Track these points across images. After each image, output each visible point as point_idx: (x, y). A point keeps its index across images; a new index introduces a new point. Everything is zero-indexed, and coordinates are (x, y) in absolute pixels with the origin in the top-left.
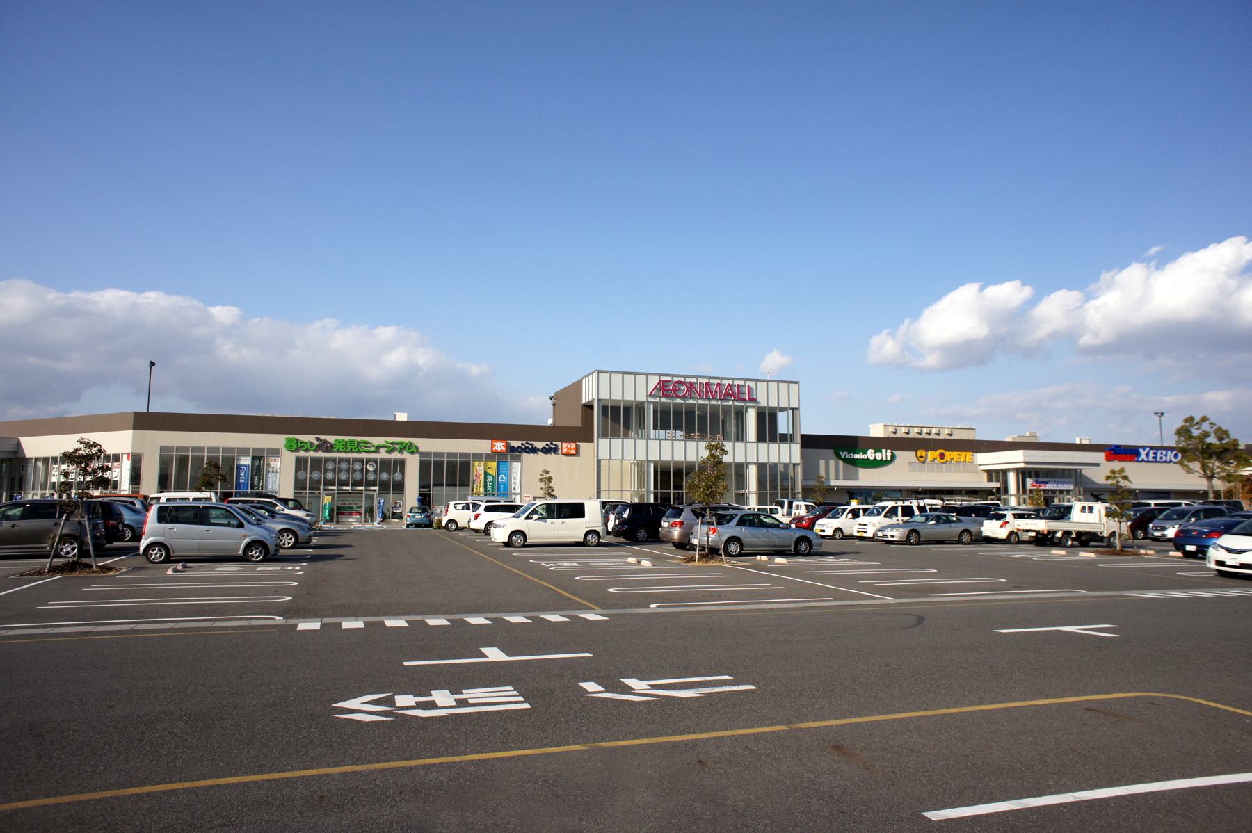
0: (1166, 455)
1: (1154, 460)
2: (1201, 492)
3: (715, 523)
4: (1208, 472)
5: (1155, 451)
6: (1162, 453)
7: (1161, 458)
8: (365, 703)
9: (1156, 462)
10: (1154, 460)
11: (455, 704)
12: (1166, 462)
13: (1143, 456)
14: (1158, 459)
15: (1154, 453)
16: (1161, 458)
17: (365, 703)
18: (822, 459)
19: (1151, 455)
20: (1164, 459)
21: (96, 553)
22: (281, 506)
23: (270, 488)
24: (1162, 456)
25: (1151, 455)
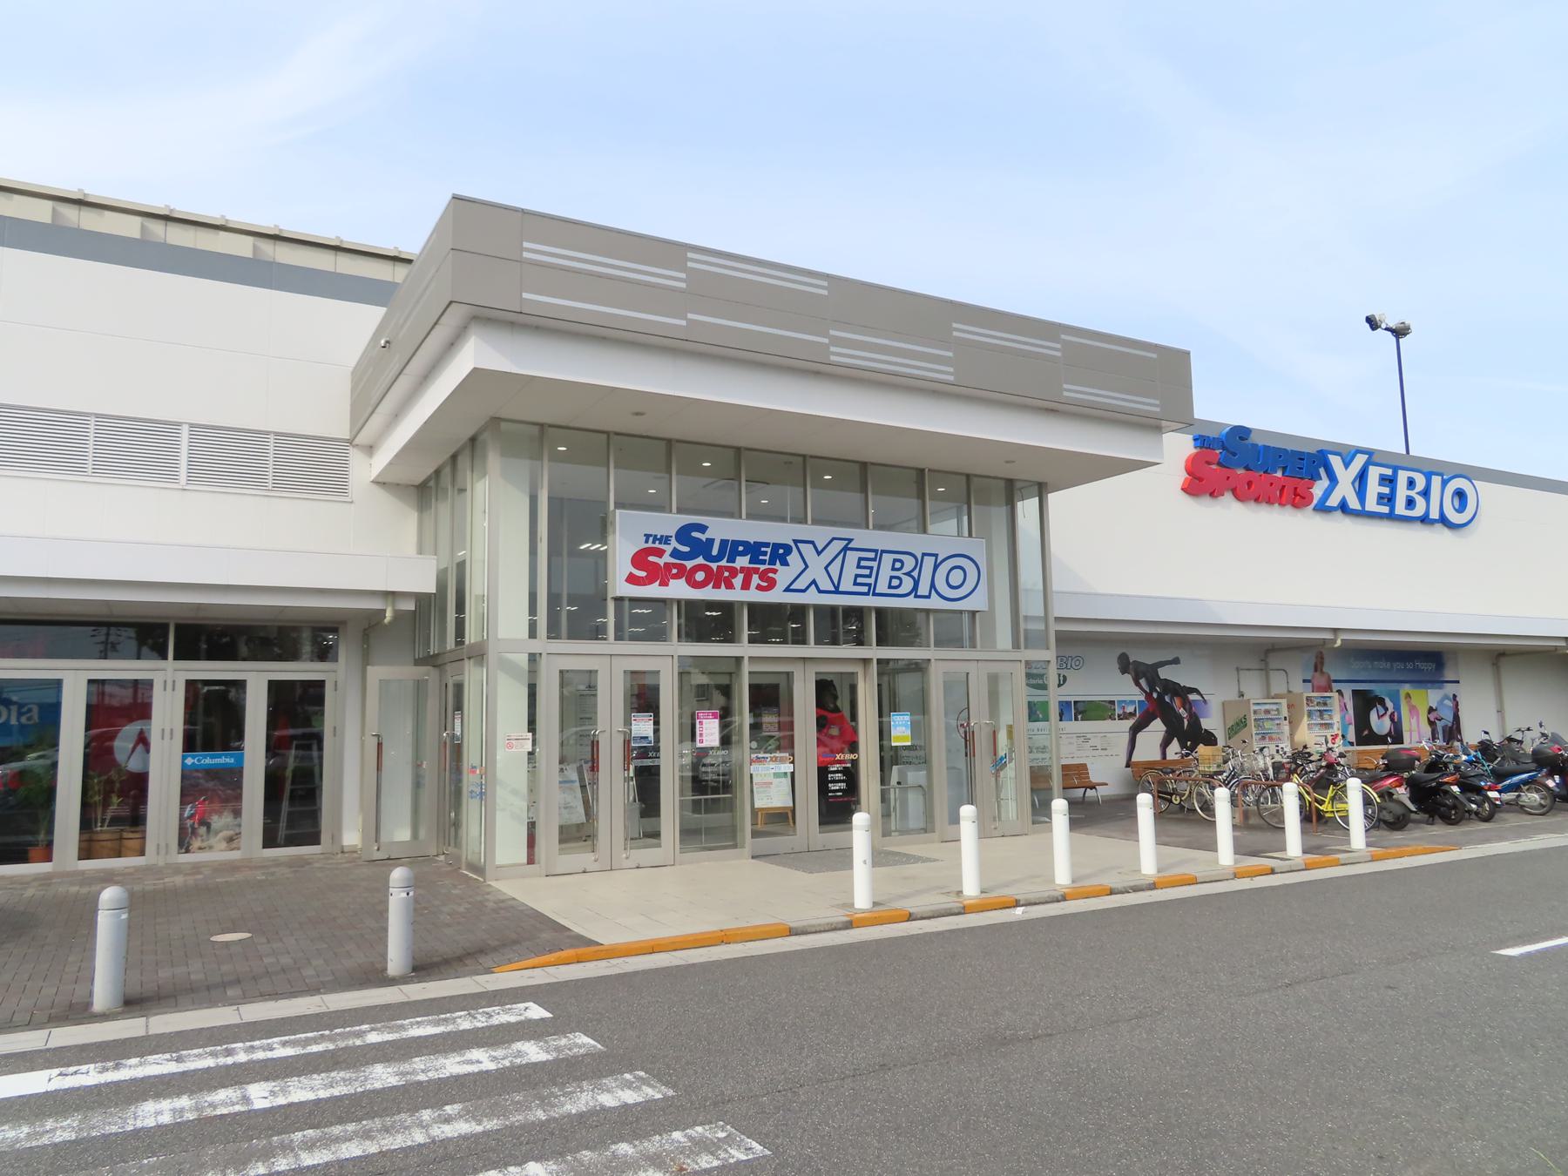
0: (1426, 493)
1: (1385, 510)
2: (219, 628)
3: (1273, 761)
4: (341, 1052)
5: (1389, 472)
6: (1411, 483)
7: (1410, 503)
8: (935, 860)
9: (1391, 517)
10: (1385, 510)
11: (1097, 787)
12: (1425, 520)
13: (1345, 490)
14: (1400, 508)
15: (1384, 480)
16: (1410, 503)
17: (935, 860)
18: (1145, 791)
19: (1374, 488)
20: (1419, 510)
21: (33, 852)
22: (1544, 793)
23: (132, 701)
24: (1412, 493)
25: (1374, 488)
